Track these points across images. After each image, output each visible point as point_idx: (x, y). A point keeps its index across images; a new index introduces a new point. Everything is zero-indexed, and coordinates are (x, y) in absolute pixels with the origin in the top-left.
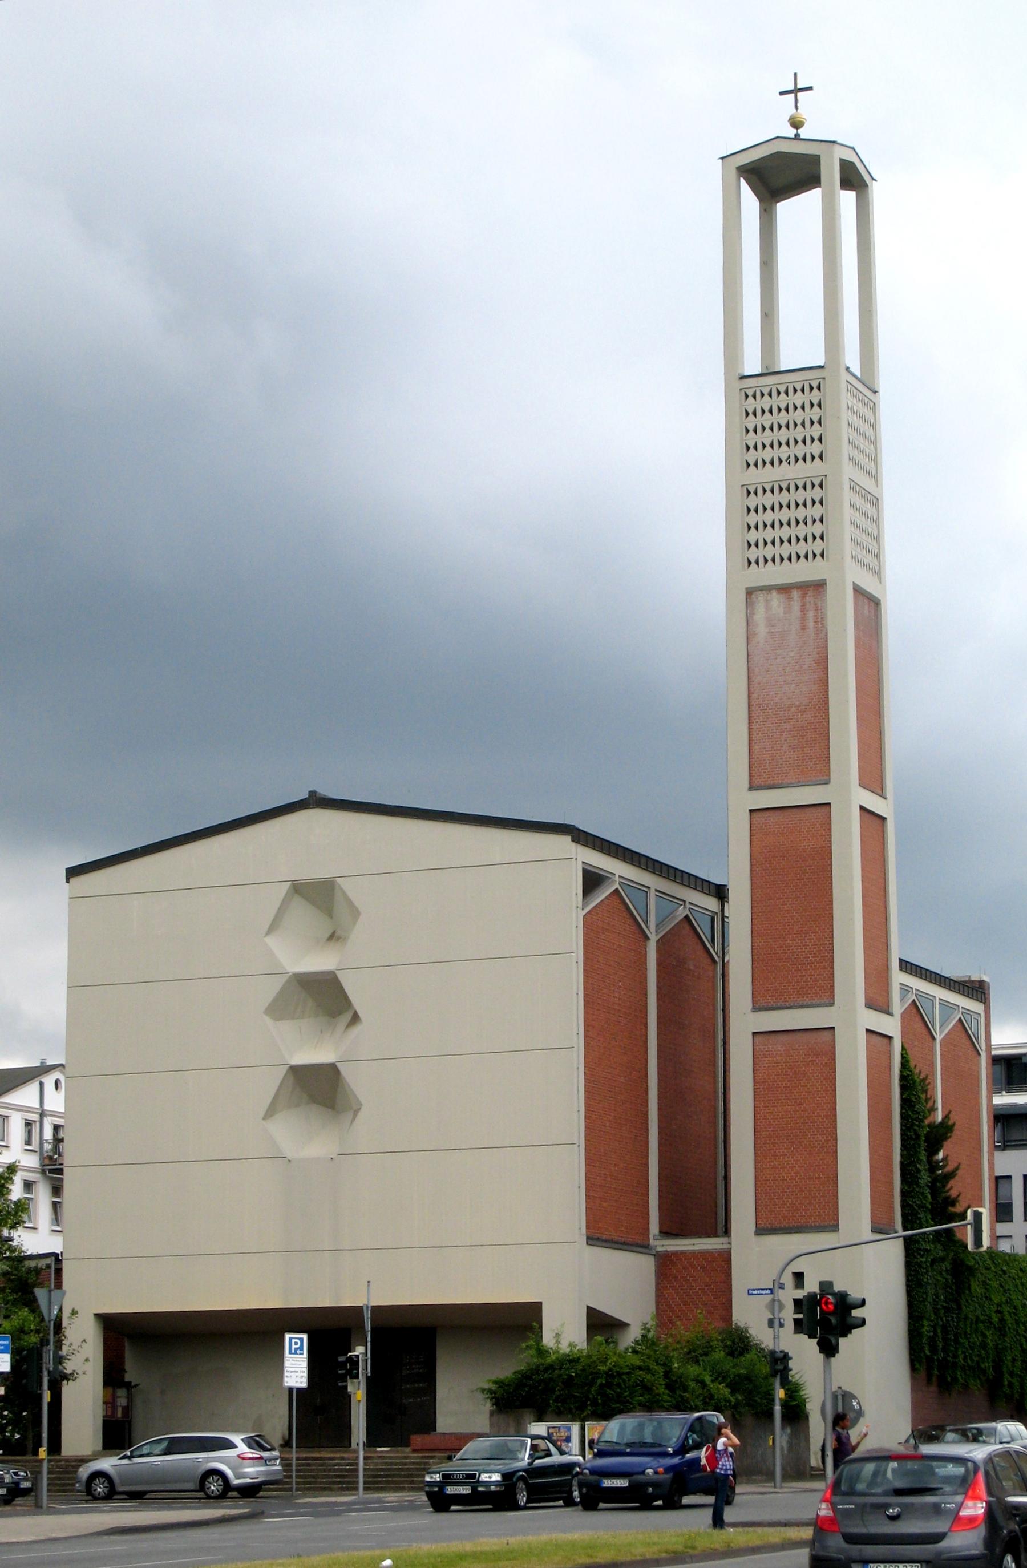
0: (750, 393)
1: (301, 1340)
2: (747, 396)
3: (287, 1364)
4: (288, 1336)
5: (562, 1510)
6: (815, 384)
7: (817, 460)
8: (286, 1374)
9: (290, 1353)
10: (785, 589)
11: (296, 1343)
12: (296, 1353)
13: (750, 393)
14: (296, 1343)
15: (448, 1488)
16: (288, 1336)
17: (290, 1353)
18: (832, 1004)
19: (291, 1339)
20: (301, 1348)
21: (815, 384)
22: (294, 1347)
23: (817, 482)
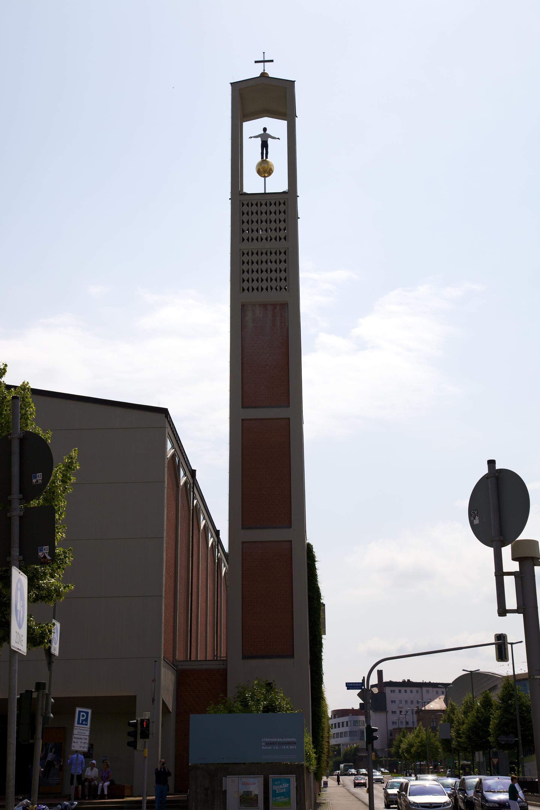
0: (245, 203)
1: (87, 713)
2: (243, 205)
3: (75, 732)
4: (78, 709)
5: (365, 806)
6: (282, 202)
7: (283, 240)
8: (74, 740)
9: (78, 723)
10: (264, 306)
11: (83, 716)
12: (82, 724)
13: (245, 203)
14: (83, 716)
15: (396, 792)
16: (78, 709)
17: (78, 723)
18: (291, 527)
19: (80, 712)
20: (86, 720)
21: (282, 202)
22: (81, 718)
23: (283, 251)
